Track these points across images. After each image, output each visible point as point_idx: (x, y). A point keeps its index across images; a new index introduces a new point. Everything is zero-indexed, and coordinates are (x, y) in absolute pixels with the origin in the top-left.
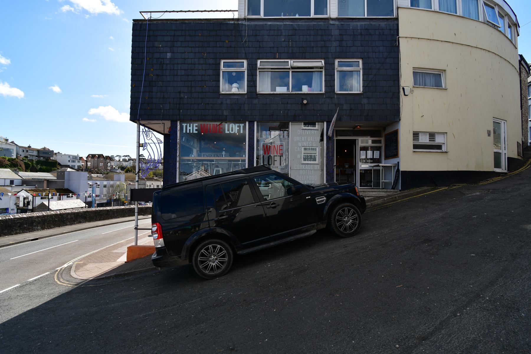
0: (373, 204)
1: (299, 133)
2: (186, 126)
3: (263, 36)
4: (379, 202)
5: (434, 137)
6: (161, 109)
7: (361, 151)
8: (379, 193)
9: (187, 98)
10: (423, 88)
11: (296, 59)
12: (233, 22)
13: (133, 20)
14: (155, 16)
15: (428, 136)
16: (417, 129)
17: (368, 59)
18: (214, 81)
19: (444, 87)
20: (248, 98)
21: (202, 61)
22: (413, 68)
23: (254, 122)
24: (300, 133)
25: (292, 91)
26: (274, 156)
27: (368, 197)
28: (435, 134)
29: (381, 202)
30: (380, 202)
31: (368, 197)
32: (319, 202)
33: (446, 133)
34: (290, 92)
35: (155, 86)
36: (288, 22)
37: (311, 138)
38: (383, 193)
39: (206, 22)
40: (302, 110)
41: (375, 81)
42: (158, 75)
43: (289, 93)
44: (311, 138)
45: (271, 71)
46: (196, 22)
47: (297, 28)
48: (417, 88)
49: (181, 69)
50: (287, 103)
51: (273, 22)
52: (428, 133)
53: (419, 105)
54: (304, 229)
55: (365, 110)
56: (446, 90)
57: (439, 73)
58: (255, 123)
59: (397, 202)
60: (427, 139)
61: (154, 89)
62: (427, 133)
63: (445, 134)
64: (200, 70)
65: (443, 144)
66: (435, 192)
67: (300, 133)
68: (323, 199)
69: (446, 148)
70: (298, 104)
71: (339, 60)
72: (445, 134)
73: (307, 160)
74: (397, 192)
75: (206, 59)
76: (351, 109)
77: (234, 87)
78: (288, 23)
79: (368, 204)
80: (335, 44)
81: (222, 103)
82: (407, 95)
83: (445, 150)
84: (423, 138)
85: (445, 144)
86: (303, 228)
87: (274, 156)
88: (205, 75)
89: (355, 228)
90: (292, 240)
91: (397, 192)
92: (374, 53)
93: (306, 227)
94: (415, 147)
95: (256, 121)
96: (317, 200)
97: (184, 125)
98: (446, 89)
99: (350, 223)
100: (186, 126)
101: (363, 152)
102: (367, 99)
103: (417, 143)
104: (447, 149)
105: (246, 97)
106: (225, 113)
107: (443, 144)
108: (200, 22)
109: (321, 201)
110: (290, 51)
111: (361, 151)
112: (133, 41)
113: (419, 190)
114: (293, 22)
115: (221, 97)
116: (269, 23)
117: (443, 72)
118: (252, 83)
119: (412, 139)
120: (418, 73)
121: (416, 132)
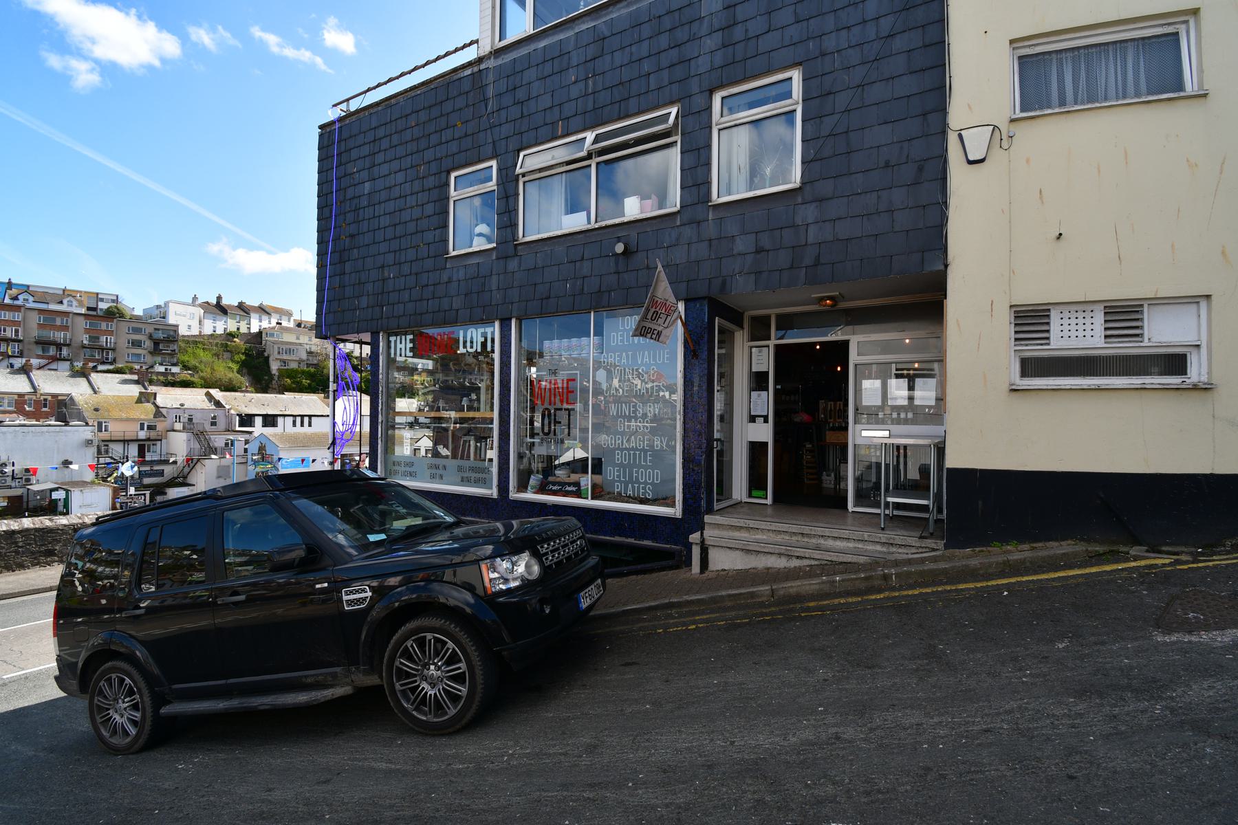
0: (782, 593)
1: (614, 343)
2: (396, 341)
3: (530, 84)
4: (807, 588)
5: (1137, 320)
6: (356, 309)
7: (752, 393)
8: (860, 546)
9: (394, 278)
10: (1065, 116)
11: (606, 125)
12: (468, 72)
13: (320, 128)
14: (354, 105)
15: (1099, 318)
16: (1031, 296)
17: (820, 59)
18: (437, 229)
19: (1190, 86)
20: (498, 259)
21: (417, 186)
22: (1012, 42)
23: (510, 319)
24: (617, 342)
25: (596, 222)
26: (556, 410)
27: (798, 557)
28: (1142, 306)
29: (817, 587)
30: (813, 587)
31: (798, 557)
32: (350, 602)
33: (1208, 297)
34: (593, 225)
35: (349, 260)
36: (584, 23)
37: (646, 352)
38: (879, 548)
39: (424, 89)
40: (617, 273)
41: (846, 132)
42: (352, 236)
43: (589, 227)
44: (646, 352)
45: (566, 172)
46: (407, 96)
47: (607, 33)
48: (1033, 121)
49: (385, 214)
50: (582, 259)
51: (550, 38)
52: (1101, 306)
53: (1041, 191)
54: (309, 680)
55: (806, 245)
56: (1202, 100)
57: (1170, 30)
58: (513, 322)
59: (956, 590)
60: (1066, 337)
61: (348, 267)
62: (1095, 307)
63: (1203, 304)
64: (414, 207)
65: (1191, 349)
66: (1054, 580)
67: (617, 342)
68: (363, 595)
69: (1204, 370)
70: (609, 256)
71: (724, 93)
72: (1203, 304)
73: (633, 420)
74: (934, 550)
75: (423, 178)
76: (759, 250)
77: (480, 235)
78: (584, 27)
79: (761, 589)
80: (710, 43)
81: (450, 281)
82: (982, 161)
83: (1204, 378)
84: (1081, 327)
85: (1204, 350)
86: (306, 677)
87: (556, 410)
88: (421, 218)
89: (435, 720)
90: (262, 708)
91: (934, 550)
92: (844, 32)
93: (313, 675)
94: (1031, 367)
95: (514, 317)
96: (345, 598)
97: (392, 339)
98: (1205, 95)
99: (423, 688)
100: (396, 341)
101: (759, 396)
102: (814, 205)
103: (1035, 350)
104: (1209, 373)
105: (494, 257)
106: (457, 303)
107: (1194, 351)
108: (413, 94)
109: (358, 600)
110: (590, 107)
111: (752, 393)
112: (320, 172)
113: (1018, 552)
114: (596, 19)
115: (448, 266)
116: (542, 44)
117: (1186, 22)
118: (505, 219)
119: (1013, 336)
120: (1054, 56)
121: (1030, 308)
